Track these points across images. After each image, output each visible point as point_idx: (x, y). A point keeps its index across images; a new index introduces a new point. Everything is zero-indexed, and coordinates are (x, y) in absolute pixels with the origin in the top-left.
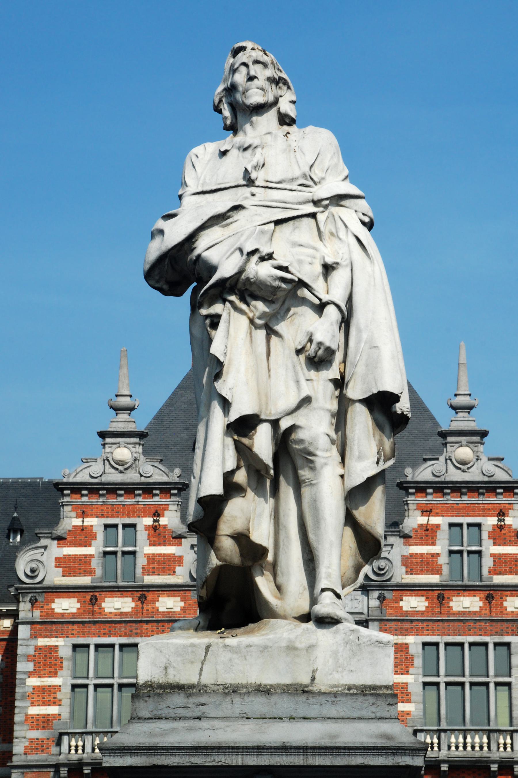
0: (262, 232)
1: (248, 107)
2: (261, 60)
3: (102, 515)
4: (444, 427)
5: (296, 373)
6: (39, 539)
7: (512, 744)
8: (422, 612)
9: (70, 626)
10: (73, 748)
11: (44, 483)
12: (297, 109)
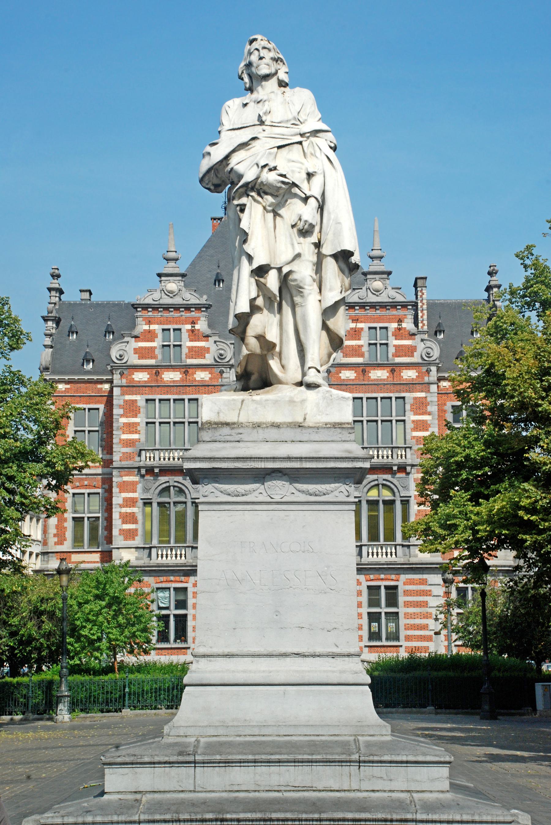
0: (270, 154)
1: (260, 76)
2: (267, 47)
3: (161, 323)
4: (365, 270)
5: (292, 239)
6: (124, 337)
7: (405, 455)
8: (353, 380)
9: (144, 388)
10: (148, 458)
11: (125, 304)
12: (289, 77)
